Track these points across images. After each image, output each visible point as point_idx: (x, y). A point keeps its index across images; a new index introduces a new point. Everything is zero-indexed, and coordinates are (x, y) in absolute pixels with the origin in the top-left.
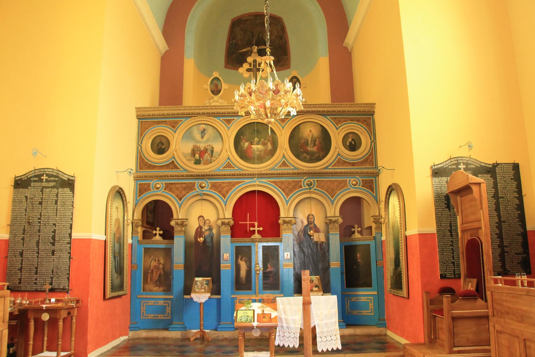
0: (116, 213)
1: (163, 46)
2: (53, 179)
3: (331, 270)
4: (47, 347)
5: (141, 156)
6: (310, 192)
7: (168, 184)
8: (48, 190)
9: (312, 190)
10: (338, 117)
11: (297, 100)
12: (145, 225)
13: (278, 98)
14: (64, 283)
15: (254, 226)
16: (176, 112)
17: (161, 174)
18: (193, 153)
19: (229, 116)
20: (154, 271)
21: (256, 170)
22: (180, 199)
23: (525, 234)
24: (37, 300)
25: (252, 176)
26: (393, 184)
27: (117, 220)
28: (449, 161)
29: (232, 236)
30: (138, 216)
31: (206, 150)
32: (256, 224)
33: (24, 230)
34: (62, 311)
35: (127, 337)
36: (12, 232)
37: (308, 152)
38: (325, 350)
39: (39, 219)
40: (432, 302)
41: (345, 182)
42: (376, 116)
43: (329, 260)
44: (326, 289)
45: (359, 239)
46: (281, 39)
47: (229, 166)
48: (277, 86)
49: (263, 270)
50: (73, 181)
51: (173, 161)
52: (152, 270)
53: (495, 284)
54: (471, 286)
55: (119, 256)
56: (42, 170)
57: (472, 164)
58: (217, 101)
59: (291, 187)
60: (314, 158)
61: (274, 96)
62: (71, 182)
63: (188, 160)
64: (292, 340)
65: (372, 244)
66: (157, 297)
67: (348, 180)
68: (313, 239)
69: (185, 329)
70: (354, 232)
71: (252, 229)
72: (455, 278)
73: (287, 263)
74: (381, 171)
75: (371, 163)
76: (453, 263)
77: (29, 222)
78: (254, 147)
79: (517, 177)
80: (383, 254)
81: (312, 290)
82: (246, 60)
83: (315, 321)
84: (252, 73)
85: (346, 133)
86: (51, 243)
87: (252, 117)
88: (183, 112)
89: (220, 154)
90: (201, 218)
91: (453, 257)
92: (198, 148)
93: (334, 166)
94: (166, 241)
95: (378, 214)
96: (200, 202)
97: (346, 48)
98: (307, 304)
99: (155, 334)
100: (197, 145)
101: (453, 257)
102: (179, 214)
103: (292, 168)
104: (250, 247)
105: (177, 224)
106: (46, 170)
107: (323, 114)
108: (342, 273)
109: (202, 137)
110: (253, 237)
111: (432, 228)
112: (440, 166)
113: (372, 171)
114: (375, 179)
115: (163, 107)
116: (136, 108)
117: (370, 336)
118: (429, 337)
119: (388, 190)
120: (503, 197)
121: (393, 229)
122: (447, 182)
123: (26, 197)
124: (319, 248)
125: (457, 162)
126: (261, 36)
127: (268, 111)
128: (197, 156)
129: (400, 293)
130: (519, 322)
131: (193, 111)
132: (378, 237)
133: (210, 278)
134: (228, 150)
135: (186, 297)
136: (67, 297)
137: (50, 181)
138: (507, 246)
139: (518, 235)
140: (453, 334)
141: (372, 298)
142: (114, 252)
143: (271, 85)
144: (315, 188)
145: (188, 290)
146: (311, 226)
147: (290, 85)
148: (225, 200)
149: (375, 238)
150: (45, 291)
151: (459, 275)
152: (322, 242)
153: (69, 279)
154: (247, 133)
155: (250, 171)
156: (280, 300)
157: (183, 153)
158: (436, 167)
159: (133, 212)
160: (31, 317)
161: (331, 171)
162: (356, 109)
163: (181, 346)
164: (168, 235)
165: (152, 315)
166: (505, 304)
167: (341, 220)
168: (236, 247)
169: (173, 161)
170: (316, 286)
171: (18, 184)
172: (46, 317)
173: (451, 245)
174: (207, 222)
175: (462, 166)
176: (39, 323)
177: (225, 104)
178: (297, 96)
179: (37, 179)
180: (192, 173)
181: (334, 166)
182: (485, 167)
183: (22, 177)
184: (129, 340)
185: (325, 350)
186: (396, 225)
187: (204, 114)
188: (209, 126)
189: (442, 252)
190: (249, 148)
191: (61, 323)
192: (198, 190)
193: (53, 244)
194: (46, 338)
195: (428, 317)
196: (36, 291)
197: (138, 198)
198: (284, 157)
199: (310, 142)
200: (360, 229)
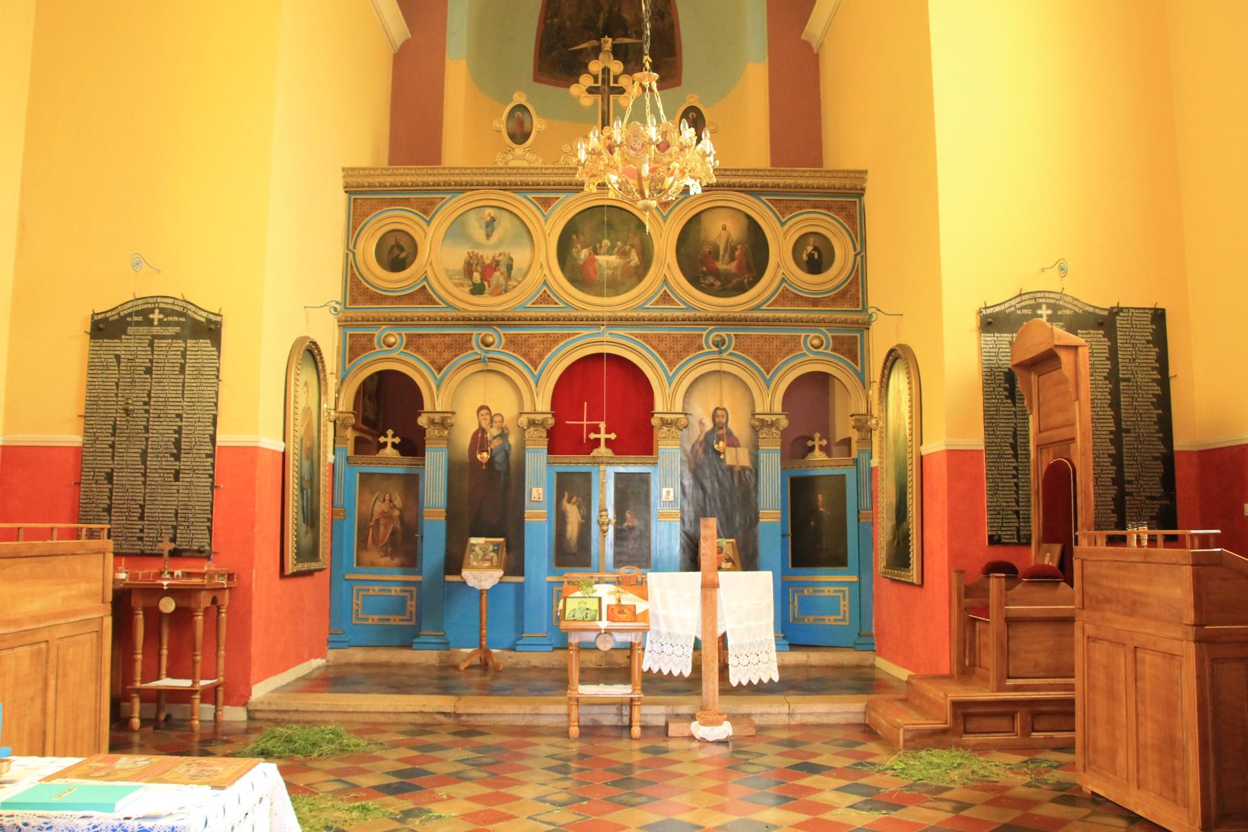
0: (305, 397)
1: (398, 29)
2: (176, 319)
3: (760, 526)
4: (168, 670)
5: (353, 274)
6: (720, 361)
7: (413, 335)
8: (164, 343)
9: (725, 355)
10: (786, 200)
11: (704, 164)
12: (361, 425)
13: (666, 159)
14: (200, 541)
15: (597, 430)
16: (431, 179)
17: (398, 315)
18: (468, 270)
19: (546, 191)
20: (382, 522)
21: (605, 309)
22: (440, 370)
23: (1169, 459)
24: (146, 571)
25: (595, 321)
26: (899, 346)
27: (307, 410)
28: (1018, 300)
29: (551, 451)
30: (346, 404)
31: (495, 265)
32: (603, 425)
33: (114, 428)
34: (203, 593)
35: (324, 661)
36: (89, 431)
37: (716, 273)
38: (745, 683)
39: (146, 403)
40: (969, 591)
41: (796, 339)
42: (867, 199)
43: (757, 505)
44: (748, 560)
45: (823, 465)
46: (662, 18)
47: (545, 299)
48: (664, 134)
49: (616, 524)
50: (218, 325)
51: (424, 287)
52: (377, 521)
53: (1089, 545)
54: (1050, 558)
55: (309, 486)
56: (151, 300)
57: (1066, 308)
58: (522, 157)
59: (678, 348)
60: (730, 286)
61: (659, 151)
62: (213, 326)
63: (456, 285)
64: (676, 660)
65: (850, 474)
66: (387, 579)
67: (803, 335)
68: (724, 460)
69: (446, 645)
70: (812, 449)
71: (593, 436)
72: (1019, 544)
73: (667, 510)
74: (874, 317)
75: (855, 300)
76: (1017, 513)
77: (127, 411)
78: (602, 259)
79: (1160, 338)
80: (873, 496)
81: (720, 568)
82: (586, 65)
83: (725, 624)
84: (599, 97)
85: (797, 239)
86: (172, 455)
87: (611, 195)
88: (446, 179)
89: (527, 272)
90: (483, 412)
91: (1017, 502)
92: (479, 259)
93: (772, 304)
94: (407, 459)
95: (864, 412)
96: (481, 377)
97: (807, 45)
98: (709, 586)
99: (383, 655)
100: (476, 251)
101: (1017, 502)
102: (435, 400)
103: (683, 306)
104: (587, 476)
105: (432, 422)
106: (159, 300)
107: (753, 191)
108: (784, 536)
109: (488, 236)
110: (595, 453)
111: (976, 440)
112: (997, 309)
113: (855, 317)
114: (862, 337)
115: (402, 169)
116: (344, 169)
117: (839, 667)
118: (961, 662)
119: (887, 360)
120: (1128, 380)
121: (895, 442)
122: (1011, 343)
123: (118, 357)
124: (736, 480)
125: (1032, 303)
126: (616, 9)
127: (646, 185)
128: (477, 277)
129: (902, 575)
130: (1128, 615)
131: (468, 179)
132: (863, 458)
133: (502, 540)
134: (545, 266)
135: (449, 578)
136: (207, 567)
137: (168, 324)
138: (1131, 482)
139: (1155, 459)
140: (1006, 653)
141: (846, 589)
142: (301, 479)
143: (652, 132)
144: (731, 350)
145: (454, 563)
146: (720, 432)
147: (689, 133)
148: (536, 373)
149: (856, 461)
150: (160, 555)
151: (1029, 537)
152: (743, 468)
153: (210, 531)
154: (587, 230)
155: (592, 312)
156: (652, 578)
157: (447, 270)
158: (989, 311)
159: (339, 399)
160: (138, 603)
161: (767, 315)
162: (825, 182)
163: (442, 678)
164: (413, 446)
165: (376, 617)
166: (1105, 582)
167: (784, 422)
168: (559, 474)
169: (424, 287)
170: (729, 560)
171: (100, 329)
172: (168, 605)
173: (1015, 476)
174: (497, 419)
175: (1044, 312)
176: (154, 616)
177: (536, 165)
178: (704, 155)
179: (140, 319)
180: (466, 314)
181: (772, 304)
182: (1094, 314)
183: (108, 314)
184: (328, 667)
185: (745, 683)
186: (902, 434)
187: (483, 185)
188: (503, 213)
189: (994, 490)
190: (591, 260)
191: (200, 618)
192: (477, 350)
193: (177, 457)
194: (165, 652)
195: (959, 619)
196: (143, 554)
197: (347, 366)
198: (665, 281)
199: (721, 253)
200: (824, 442)
